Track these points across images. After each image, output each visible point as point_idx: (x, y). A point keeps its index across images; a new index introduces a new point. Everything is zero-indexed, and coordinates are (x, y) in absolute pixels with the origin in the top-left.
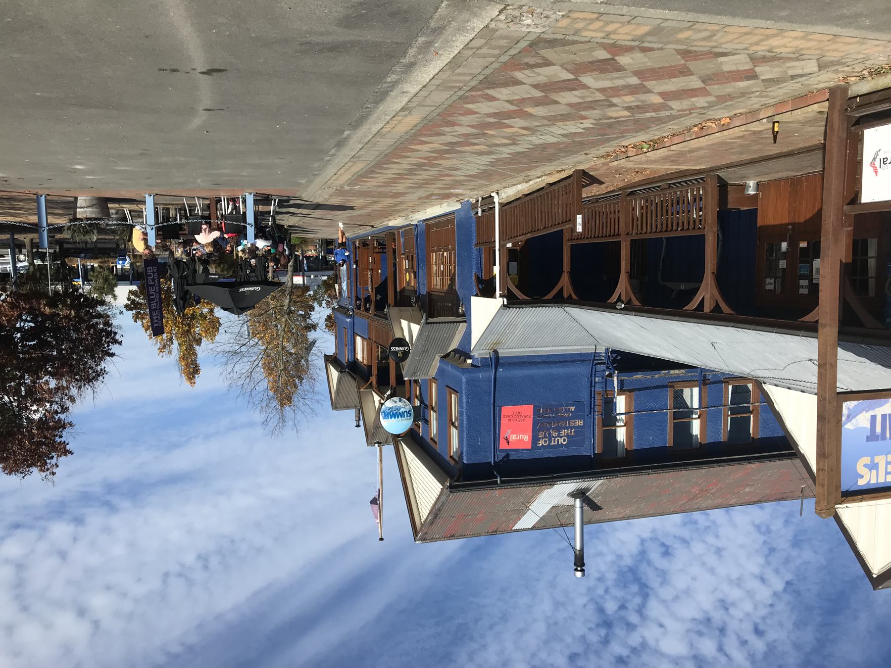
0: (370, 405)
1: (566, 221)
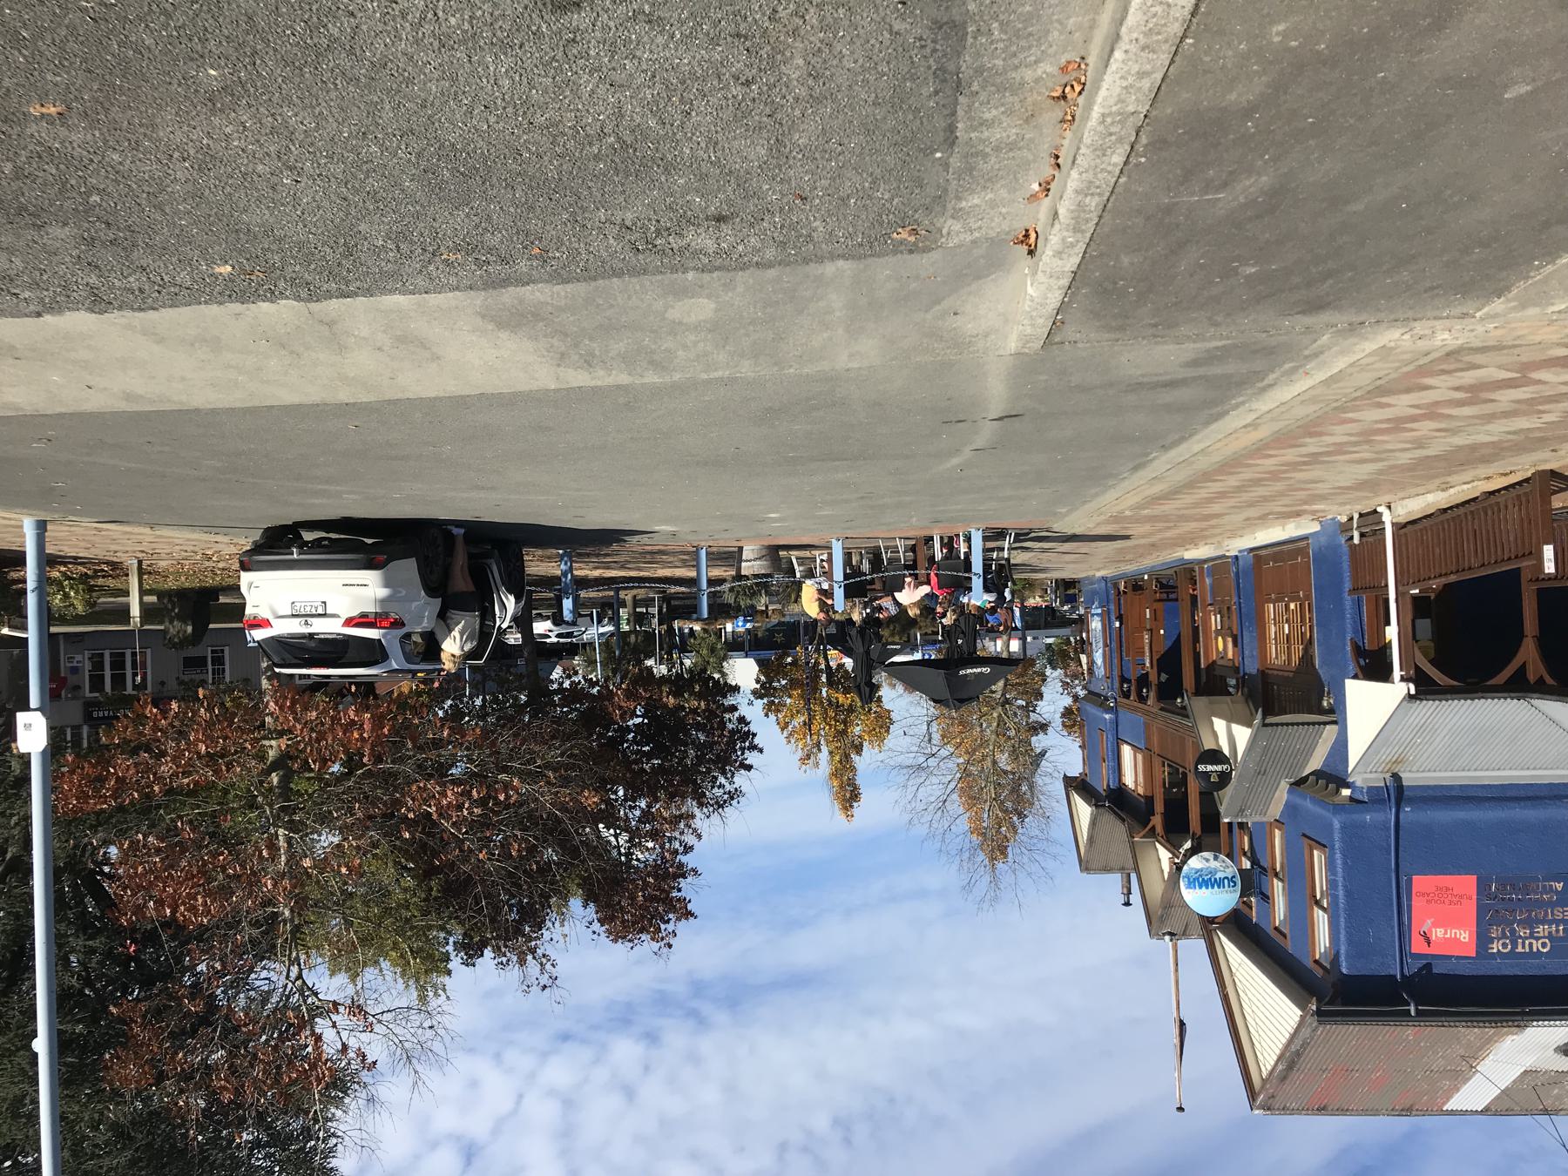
0: (1154, 867)
1: (1524, 555)
